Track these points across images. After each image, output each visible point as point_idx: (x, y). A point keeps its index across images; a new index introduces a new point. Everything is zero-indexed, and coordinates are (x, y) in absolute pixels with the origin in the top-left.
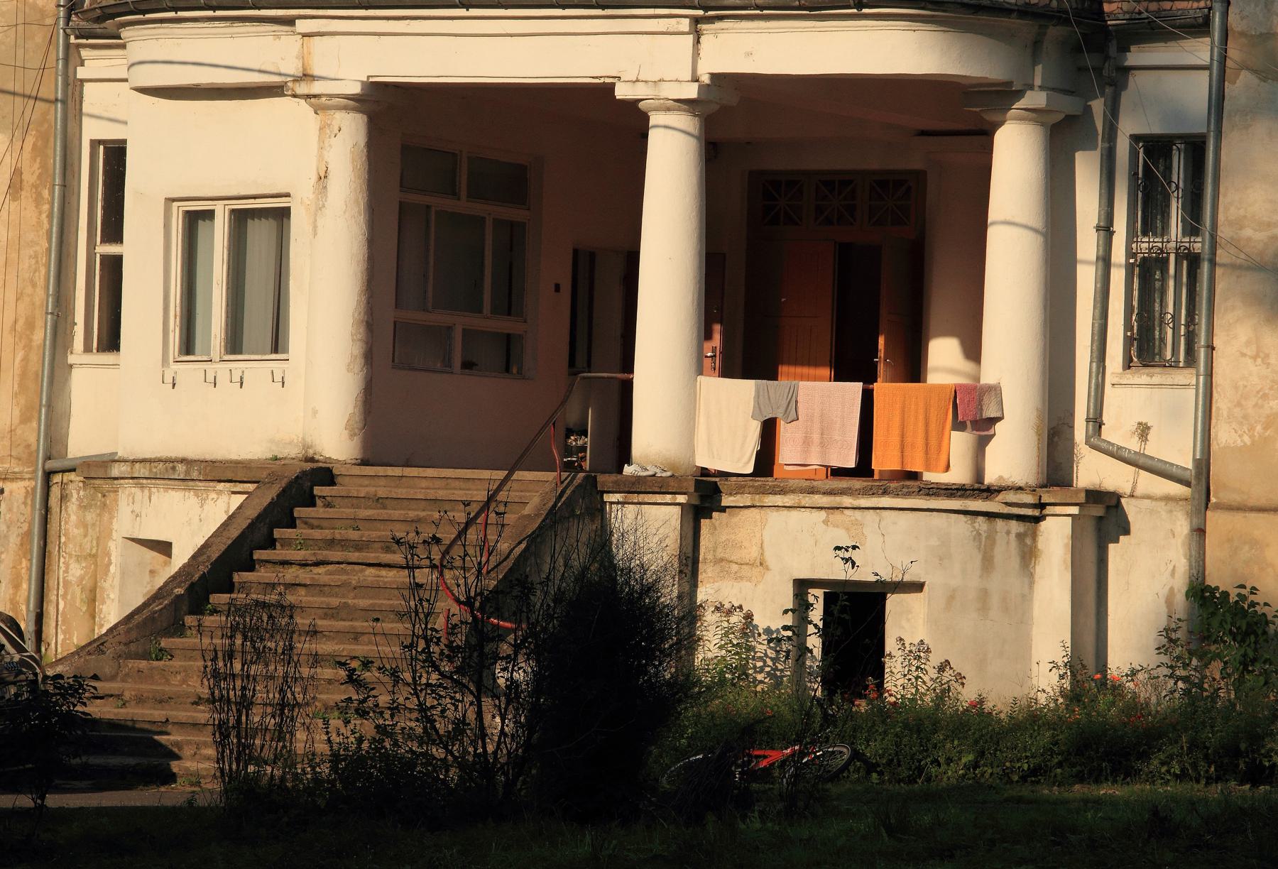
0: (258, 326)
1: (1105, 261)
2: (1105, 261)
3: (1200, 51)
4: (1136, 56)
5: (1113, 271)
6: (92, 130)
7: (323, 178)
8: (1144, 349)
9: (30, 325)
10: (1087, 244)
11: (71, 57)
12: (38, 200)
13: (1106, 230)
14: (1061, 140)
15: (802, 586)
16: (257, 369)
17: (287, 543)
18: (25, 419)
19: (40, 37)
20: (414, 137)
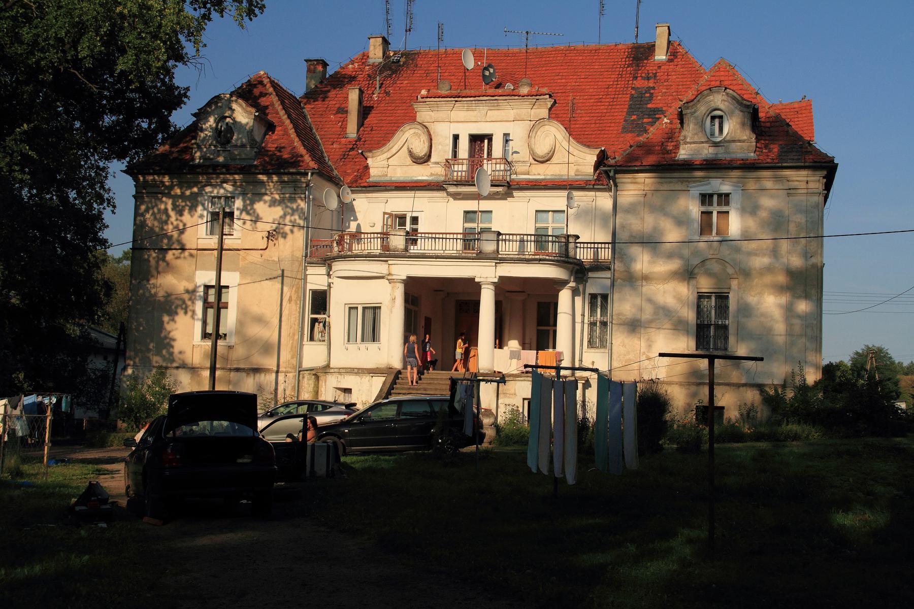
0: (372, 333)
1: (583, 322)
2: (583, 322)
3: (608, 274)
4: (590, 275)
5: (576, 324)
6: (310, 287)
7: (394, 299)
8: (591, 344)
9: (294, 335)
10: (578, 318)
11: (306, 270)
12: (296, 304)
13: (583, 315)
14: (575, 292)
15: (524, 399)
16: (373, 346)
17: (397, 389)
18: (292, 358)
19: (297, 264)
20: (416, 291)
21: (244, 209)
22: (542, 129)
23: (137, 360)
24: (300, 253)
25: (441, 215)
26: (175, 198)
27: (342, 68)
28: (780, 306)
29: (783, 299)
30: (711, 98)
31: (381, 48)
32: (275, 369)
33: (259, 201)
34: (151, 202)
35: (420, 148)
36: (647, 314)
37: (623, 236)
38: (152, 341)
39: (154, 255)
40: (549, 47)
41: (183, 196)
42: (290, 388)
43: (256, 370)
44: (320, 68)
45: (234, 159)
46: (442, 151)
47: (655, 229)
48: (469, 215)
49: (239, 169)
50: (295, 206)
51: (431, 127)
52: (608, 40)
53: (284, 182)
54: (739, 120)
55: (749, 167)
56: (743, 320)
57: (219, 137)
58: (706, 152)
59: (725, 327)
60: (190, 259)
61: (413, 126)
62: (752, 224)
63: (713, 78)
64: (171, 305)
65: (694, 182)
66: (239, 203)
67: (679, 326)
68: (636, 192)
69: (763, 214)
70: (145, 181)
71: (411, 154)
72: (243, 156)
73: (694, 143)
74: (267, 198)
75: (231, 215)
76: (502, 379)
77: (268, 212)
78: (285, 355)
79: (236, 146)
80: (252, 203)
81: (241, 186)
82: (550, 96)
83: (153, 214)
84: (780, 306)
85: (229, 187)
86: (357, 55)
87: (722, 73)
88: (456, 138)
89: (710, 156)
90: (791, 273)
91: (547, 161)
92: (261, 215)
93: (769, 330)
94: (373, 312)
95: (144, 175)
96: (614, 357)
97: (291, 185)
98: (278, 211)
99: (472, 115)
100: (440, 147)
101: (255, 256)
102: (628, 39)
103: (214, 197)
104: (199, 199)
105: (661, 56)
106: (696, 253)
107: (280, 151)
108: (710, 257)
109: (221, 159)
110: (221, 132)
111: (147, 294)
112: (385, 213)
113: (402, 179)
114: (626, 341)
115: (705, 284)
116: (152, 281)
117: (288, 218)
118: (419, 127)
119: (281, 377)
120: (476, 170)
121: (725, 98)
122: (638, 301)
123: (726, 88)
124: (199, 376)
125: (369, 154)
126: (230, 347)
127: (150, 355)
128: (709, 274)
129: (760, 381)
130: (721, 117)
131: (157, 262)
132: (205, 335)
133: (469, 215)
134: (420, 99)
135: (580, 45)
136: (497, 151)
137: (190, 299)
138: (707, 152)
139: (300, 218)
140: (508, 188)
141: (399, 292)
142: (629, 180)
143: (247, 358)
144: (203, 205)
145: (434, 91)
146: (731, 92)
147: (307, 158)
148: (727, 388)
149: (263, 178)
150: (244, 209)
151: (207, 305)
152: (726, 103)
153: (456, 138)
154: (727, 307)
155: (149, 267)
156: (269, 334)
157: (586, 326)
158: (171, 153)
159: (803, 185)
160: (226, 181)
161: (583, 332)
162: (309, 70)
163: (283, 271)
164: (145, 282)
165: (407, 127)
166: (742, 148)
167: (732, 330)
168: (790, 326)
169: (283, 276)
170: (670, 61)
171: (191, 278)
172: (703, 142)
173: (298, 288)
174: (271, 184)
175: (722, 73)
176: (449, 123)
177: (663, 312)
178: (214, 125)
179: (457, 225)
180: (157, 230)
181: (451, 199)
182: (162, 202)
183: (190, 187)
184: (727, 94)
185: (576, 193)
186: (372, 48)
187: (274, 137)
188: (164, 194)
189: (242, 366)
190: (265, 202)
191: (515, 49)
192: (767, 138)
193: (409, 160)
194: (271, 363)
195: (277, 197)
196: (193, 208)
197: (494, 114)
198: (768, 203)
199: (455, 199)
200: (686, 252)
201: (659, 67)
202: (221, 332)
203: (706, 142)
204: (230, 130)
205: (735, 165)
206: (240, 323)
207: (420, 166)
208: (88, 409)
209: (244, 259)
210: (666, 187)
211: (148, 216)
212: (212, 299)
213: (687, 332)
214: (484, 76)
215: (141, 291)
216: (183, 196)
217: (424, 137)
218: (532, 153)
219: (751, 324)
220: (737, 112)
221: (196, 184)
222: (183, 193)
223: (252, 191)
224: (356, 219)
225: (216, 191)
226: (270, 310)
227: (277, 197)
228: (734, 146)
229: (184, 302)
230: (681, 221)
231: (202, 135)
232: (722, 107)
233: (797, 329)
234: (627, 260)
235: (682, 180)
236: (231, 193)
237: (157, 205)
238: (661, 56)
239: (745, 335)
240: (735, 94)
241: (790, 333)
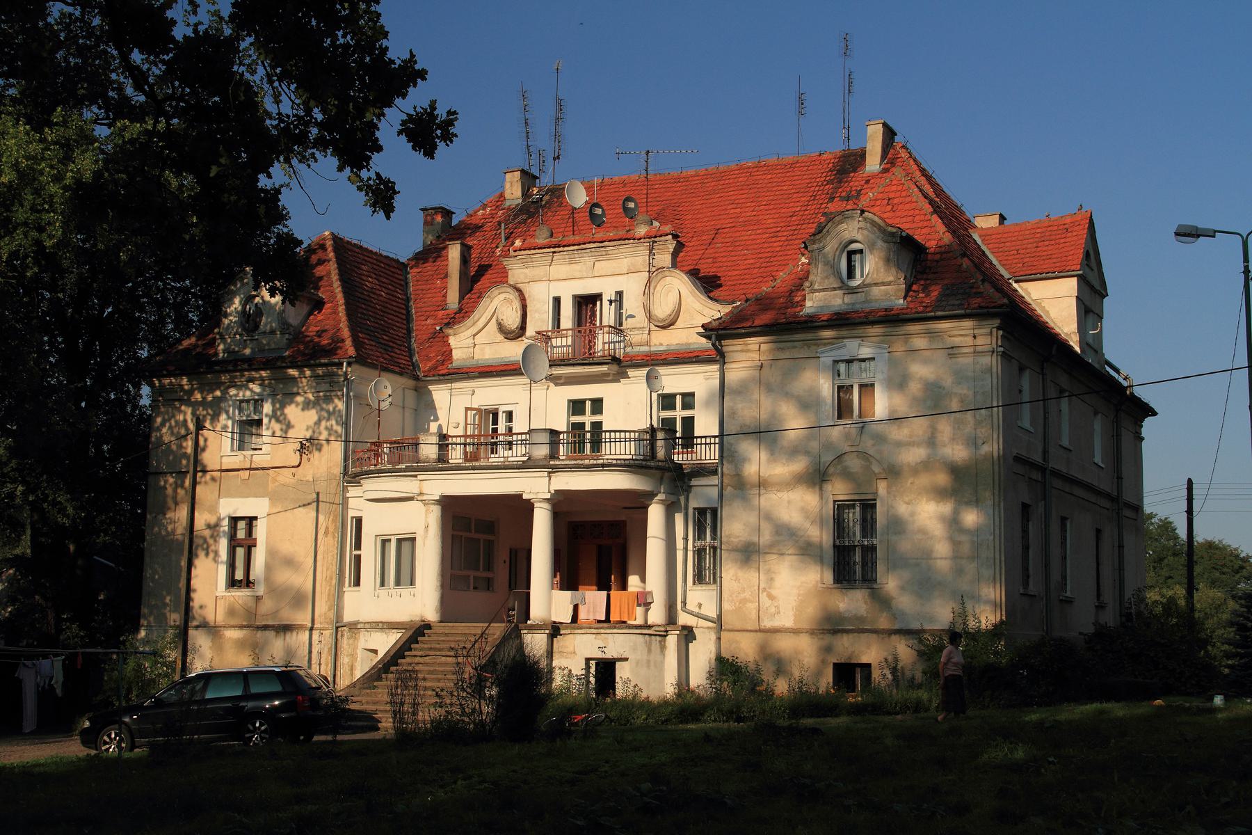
0: (405, 576)
1: (686, 549)
2: (686, 549)
3: (714, 480)
4: (694, 482)
7: (427, 527)
8: (699, 578)
11: (345, 490)
13: (686, 539)
14: (671, 509)
16: (405, 591)
19: (335, 484)
21: (274, 416)
22: (662, 283)
23: (151, 619)
24: (338, 470)
25: (542, 406)
26: (195, 405)
27: (470, 216)
29: (946, 508)
30: (844, 226)
31: (519, 184)
33: (292, 402)
34: (167, 413)
36: (766, 537)
37: (730, 428)
38: (169, 594)
39: (171, 480)
41: (203, 403)
42: (326, 649)
44: (439, 219)
45: (262, 350)
46: (539, 320)
47: (773, 415)
48: (577, 406)
49: (264, 364)
51: (527, 289)
53: (318, 376)
54: (883, 254)
55: (892, 319)
56: (894, 538)
57: (247, 322)
59: (873, 549)
60: (212, 484)
61: (503, 290)
62: (901, 404)
63: (880, 196)
64: (192, 545)
65: (825, 345)
66: (267, 408)
67: (807, 551)
69: (915, 387)
71: (501, 328)
72: (273, 346)
74: (299, 399)
76: (568, 629)
77: (301, 418)
78: (322, 607)
79: (264, 333)
80: (283, 407)
81: (270, 386)
82: (675, 237)
83: (171, 428)
84: (942, 519)
85: (256, 388)
88: (557, 301)
89: (844, 308)
90: (956, 471)
92: (293, 422)
93: (928, 555)
94: (407, 543)
95: (159, 377)
96: (725, 595)
97: (327, 379)
98: (312, 415)
99: (576, 269)
100: (537, 315)
101: (285, 476)
103: (241, 401)
104: (222, 405)
105: (873, 163)
106: (828, 446)
107: (320, 336)
108: (848, 449)
109: (248, 351)
110: (249, 315)
111: (163, 533)
112: (467, 409)
113: (490, 363)
114: (740, 574)
115: (839, 490)
117: (323, 423)
118: (509, 290)
120: (589, 344)
121: (862, 224)
122: (752, 518)
123: (862, 212)
125: (450, 331)
126: (258, 599)
128: (847, 475)
129: (915, 625)
130: (861, 251)
131: (175, 491)
132: (232, 583)
133: (577, 406)
134: (512, 253)
135: (773, 159)
136: (607, 314)
137: (212, 536)
139: (337, 423)
140: (619, 366)
141: (436, 511)
142: (739, 348)
143: (276, 613)
144: (227, 412)
146: (870, 215)
147: (348, 342)
148: (875, 636)
149: (293, 372)
150: (274, 416)
151: (234, 543)
152: (865, 232)
153: (557, 301)
154: (874, 521)
155: (166, 496)
156: (302, 580)
157: (690, 554)
159: (969, 341)
160: (252, 380)
161: (685, 562)
162: (426, 223)
163: (318, 494)
164: (160, 517)
165: (495, 291)
166: (887, 293)
167: (880, 553)
168: (955, 543)
169: (318, 501)
170: (885, 171)
171: (213, 509)
172: (835, 289)
173: (336, 516)
174: (304, 380)
175: (894, 188)
176: (548, 281)
177: (785, 533)
179: (560, 421)
180: (174, 447)
182: (181, 411)
183: (212, 391)
184: (865, 219)
185: (662, 370)
186: (508, 186)
187: (320, 317)
188: (181, 401)
189: (270, 623)
190: (297, 404)
192: (931, 276)
193: (500, 337)
194: (303, 618)
195: (310, 396)
196: (215, 417)
197: (603, 266)
198: (921, 371)
199: (556, 384)
200: (814, 445)
202: (251, 578)
203: (840, 288)
204: (259, 312)
206: (268, 567)
207: (513, 343)
208: (954, 636)
209: (275, 480)
210: (787, 355)
212: (241, 534)
213: (821, 560)
214: (626, 209)
216: (203, 403)
217: (517, 304)
218: (650, 318)
219: (905, 546)
220: (880, 243)
221: (218, 385)
222: (204, 398)
223: (283, 392)
224: (436, 419)
226: (301, 548)
227: (310, 396)
228: (876, 291)
230: (807, 404)
231: (226, 322)
232: (859, 237)
233: (966, 549)
235: (808, 343)
236: (258, 394)
237: (174, 416)
238: (873, 163)
239: (897, 562)
241: (956, 557)
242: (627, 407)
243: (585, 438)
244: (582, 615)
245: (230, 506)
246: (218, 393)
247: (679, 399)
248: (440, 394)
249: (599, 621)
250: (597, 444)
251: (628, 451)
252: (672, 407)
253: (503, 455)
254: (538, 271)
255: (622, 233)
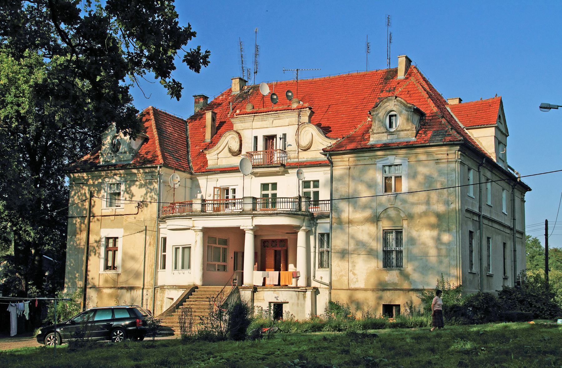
0: (186, 265)
1: (315, 252)
2: (315, 252)
3: (328, 220)
4: (319, 221)
8: (321, 265)
9: (152, 266)
10: (312, 249)
11: (158, 224)
13: (315, 247)
14: (308, 234)
16: (186, 271)
19: (154, 222)
21: (126, 191)
24: (155, 216)
25: (249, 186)
28: (433, 238)
29: (435, 233)
30: (388, 104)
32: (142, 287)
33: (134, 184)
35: (235, 147)
36: (352, 247)
40: (337, 76)
41: (93, 185)
42: (150, 298)
43: (131, 288)
44: (202, 101)
46: (248, 147)
47: (355, 191)
48: (265, 186)
49: (121, 167)
50: (152, 187)
51: (242, 133)
52: (372, 69)
55: (409, 146)
57: (114, 148)
58: (386, 138)
59: (401, 252)
60: (97, 222)
61: (231, 133)
63: (404, 90)
65: (379, 158)
66: (123, 187)
67: (371, 253)
68: (344, 167)
70: (74, 177)
71: (230, 150)
72: (125, 159)
73: (378, 133)
74: (138, 183)
75: (119, 194)
76: (261, 291)
78: (148, 278)
79: (121, 153)
80: (130, 187)
81: (124, 177)
82: (310, 109)
83: (78, 196)
84: (433, 238)
85: (118, 178)
86: (226, 90)
87: (411, 86)
88: (256, 138)
89: (388, 141)
90: (439, 216)
91: (309, 149)
94: (187, 248)
97: (150, 174)
98: (143, 191)
99: (264, 124)
100: (247, 145)
102: (385, 68)
103: (111, 184)
104: (102, 186)
105: (401, 75)
106: (380, 205)
107: (147, 154)
108: (390, 206)
109: (114, 161)
110: (115, 145)
112: (214, 188)
114: (340, 263)
115: (385, 225)
116: (78, 236)
117: (149, 194)
118: (234, 133)
119: (145, 291)
120: (271, 157)
121: (396, 103)
123: (396, 97)
124: (101, 292)
127: (77, 280)
128: (389, 218)
130: (395, 115)
132: (107, 268)
133: (265, 186)
134: (235, 116)
135: (355, 73)
137: (97, 246)
138: (385, 139)
139: (155, 194)
140: (285, 168)
141: (200, 234)
142: (339, 160)
143: (126, 282)
144: (104, 189)
145: (243, 110)
146: (400, 99)
147: (160, 157)
148: (402, 292)
150: (126, 191)
152: (397, 107)
153: (256, 138)
154: (401, 239)
156: (138, 266)
157: (317, 254)
158: (90, 159)
159: (445, 156)
160: (115, 175)
162: (196, 102)
163: (146, 227)
164: (74, 237)
165: (227, 134)
167: (404, 254)
169: (146, 230)
170: (407, 78)
171: (98, 233)
172: (383, 133)
173: (154, 237)
174: (140, 174)
175: (411, 86)
176: (251, 129)
177: (360, 244)
178: (110, 142)
181: (253, 177)
182: (83, 189)
183: (97, 179)
184: (397, 100)
185: (304, 170)
186: (233, 85)
189: (124, 286)
191: (291, 81)
193: (230, 155)
194: (139, 284)
195: (143, 182)
198: (423, 170)
199: (255, 176)
200: (374, 204)
201: (398, 83)
202: (115, 265)
203: (386, 132)
205: (400, 146)
206: (123, 261)
207: (236, 157)
209: (126, 220)
211: (76, 197)
212: (111, 245)
215: (72, 243)
217: (237, 140)
220: (404, 112)
221: (100, 176)
224: (200, 192)
225: (111, 181)
229: (94, 248)
230: (371, 185)
232: (394, 109)
234: (339, 211)
237: (80, 191)
238: (401, 75)
240: (402, 100)
242: (288, 186)
243: (268, 201)
244: (267, 282)
245: (106, 232)
246: (100, 180)
247: (312, 183)
248: (202, 181)
249: (275, 285)
250: (274, 204)
251: (289, 207)
252: (309, 187)
253: (231, 209)
254: (248, 125)
255: (285, 107)
